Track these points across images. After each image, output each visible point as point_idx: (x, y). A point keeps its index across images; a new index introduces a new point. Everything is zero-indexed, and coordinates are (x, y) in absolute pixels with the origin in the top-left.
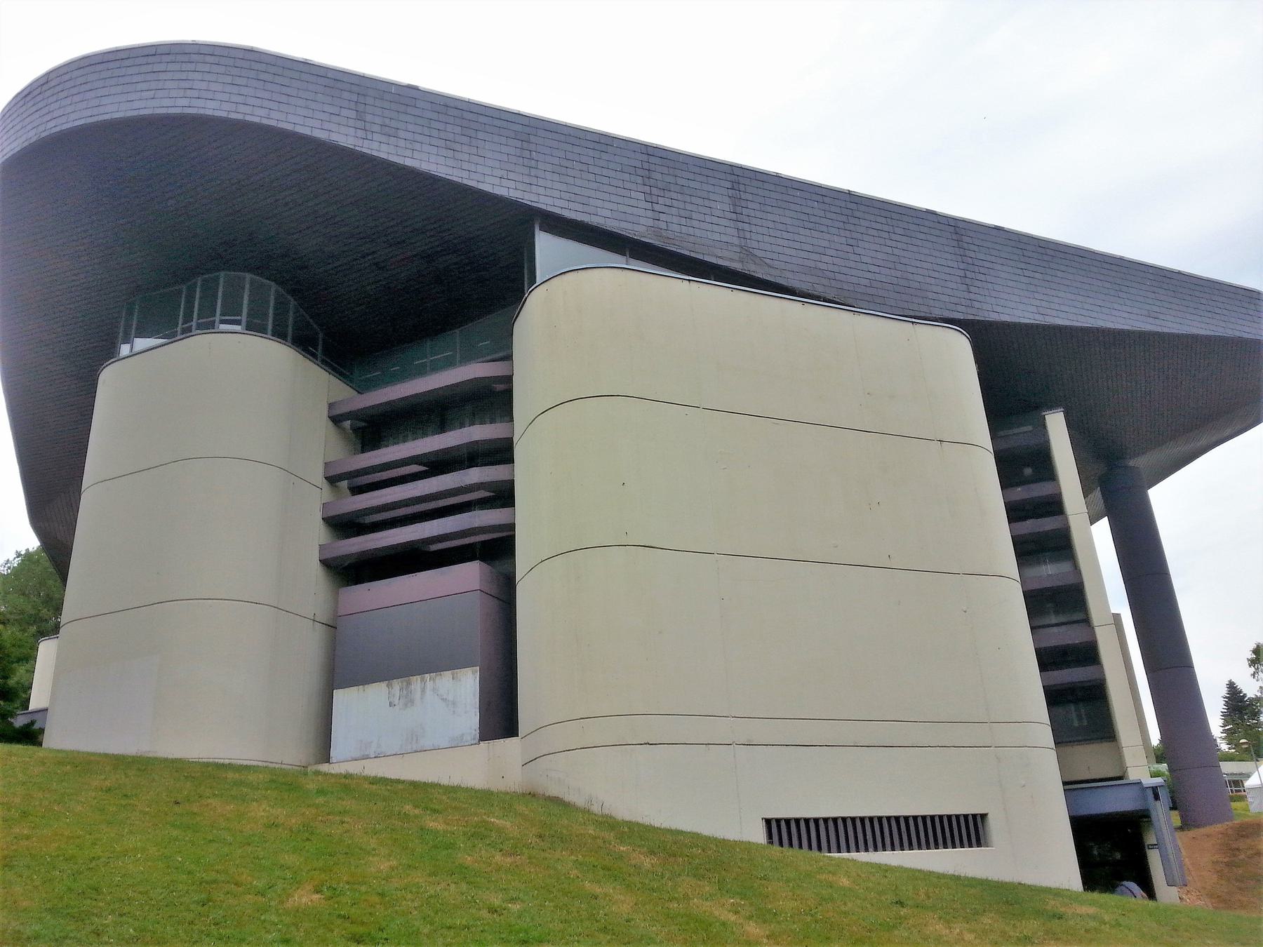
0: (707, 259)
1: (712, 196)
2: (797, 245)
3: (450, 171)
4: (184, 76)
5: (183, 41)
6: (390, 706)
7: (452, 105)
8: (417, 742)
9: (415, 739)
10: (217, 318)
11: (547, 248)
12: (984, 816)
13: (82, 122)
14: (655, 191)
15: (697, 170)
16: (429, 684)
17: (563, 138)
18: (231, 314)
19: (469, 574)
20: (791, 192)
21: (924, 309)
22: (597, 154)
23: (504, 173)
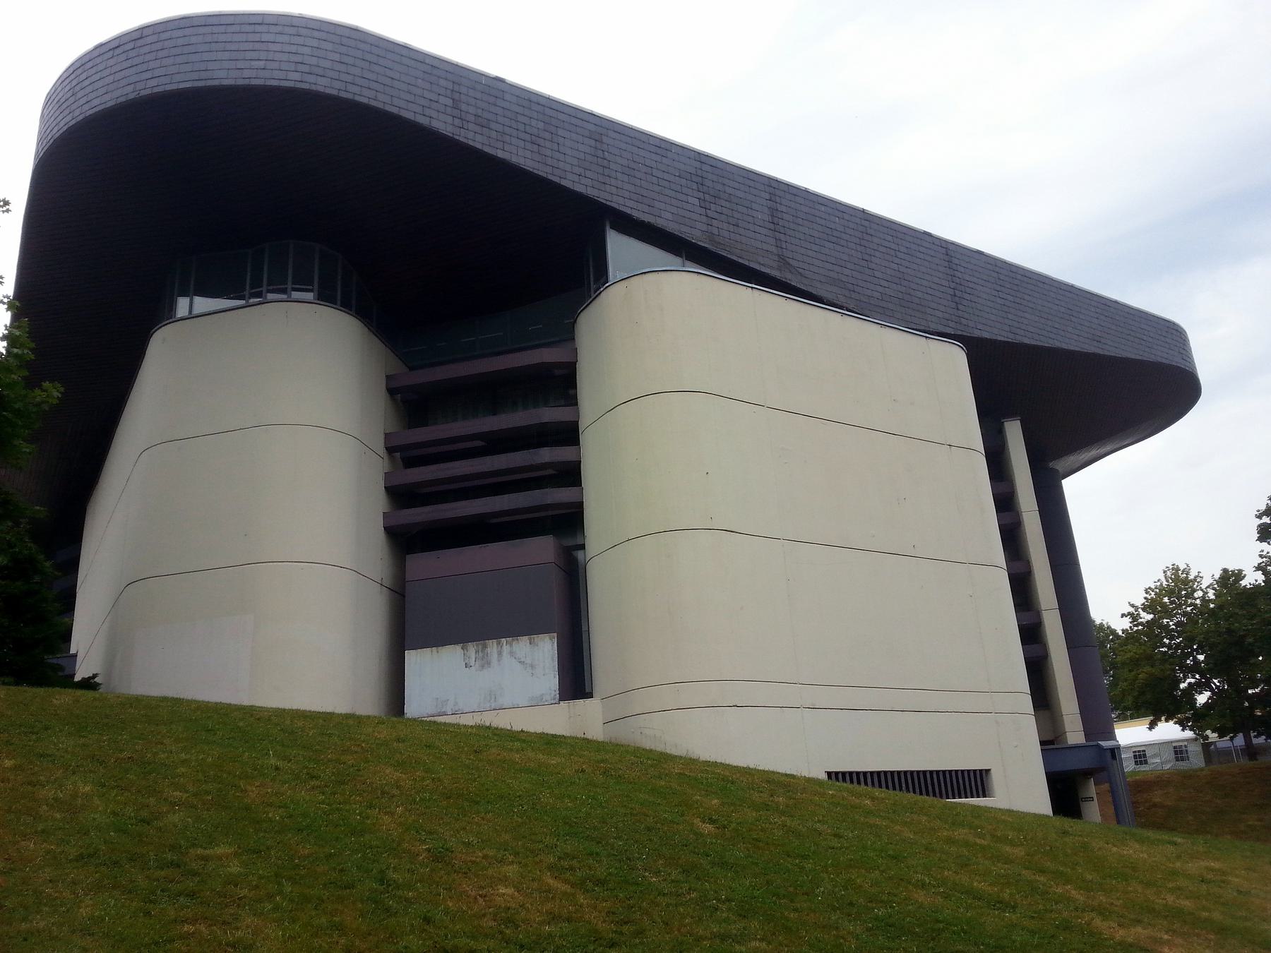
0: (753, 265)
1: (754, 206)
2: (824, 258)
3: (536, 165)
4: (293, 49)
5: (322, 18)
6: (466, 667)
7: (536, 101)
8: (495, 701)
9: (493, 697)
10: (289, 286)
11: (619, 248)
12: (988, 771)
13: (188, 85)
14: (707, 197)
15: (741, 180)
16: (506, 648)
17: (629, 140)
18: (302, 282)
19: (542, 549)
20: (818, 206)
21: (924, 323)
22: (658, 158)
23: (582, 171)
